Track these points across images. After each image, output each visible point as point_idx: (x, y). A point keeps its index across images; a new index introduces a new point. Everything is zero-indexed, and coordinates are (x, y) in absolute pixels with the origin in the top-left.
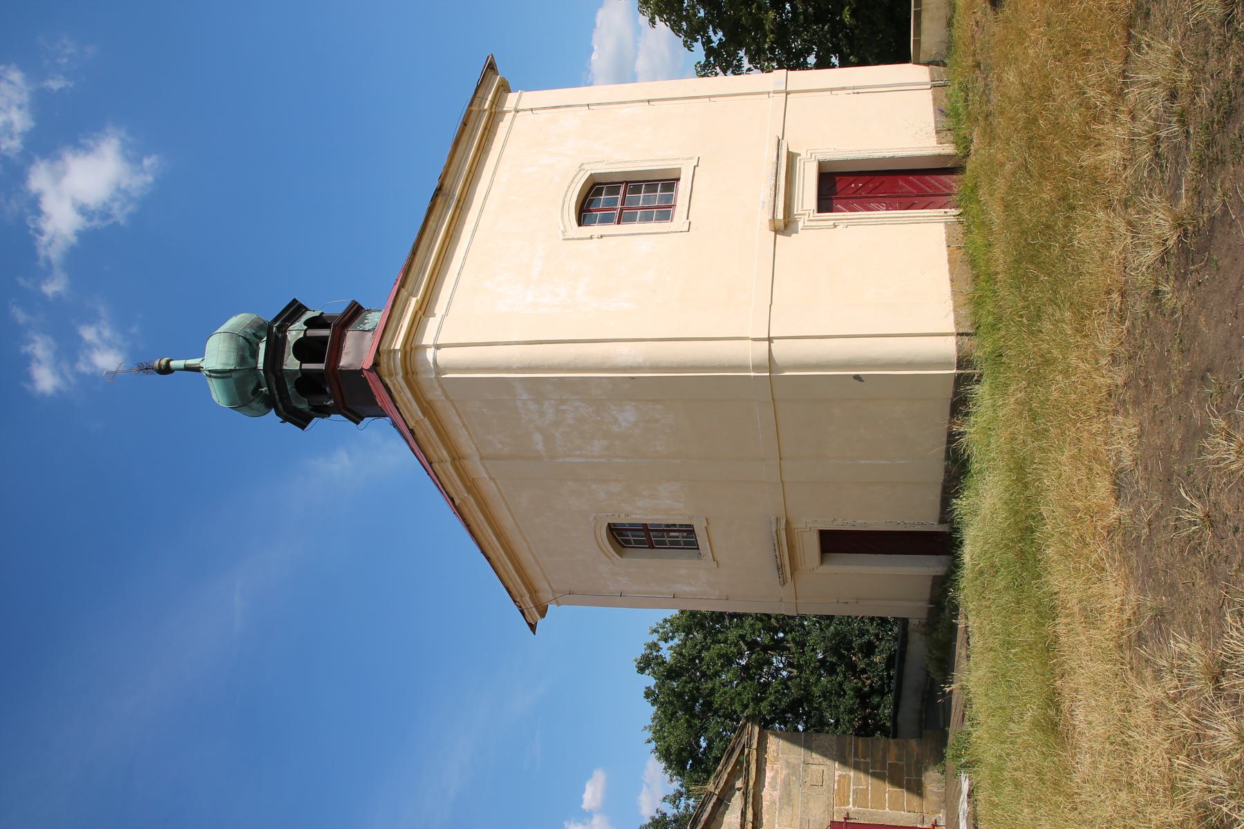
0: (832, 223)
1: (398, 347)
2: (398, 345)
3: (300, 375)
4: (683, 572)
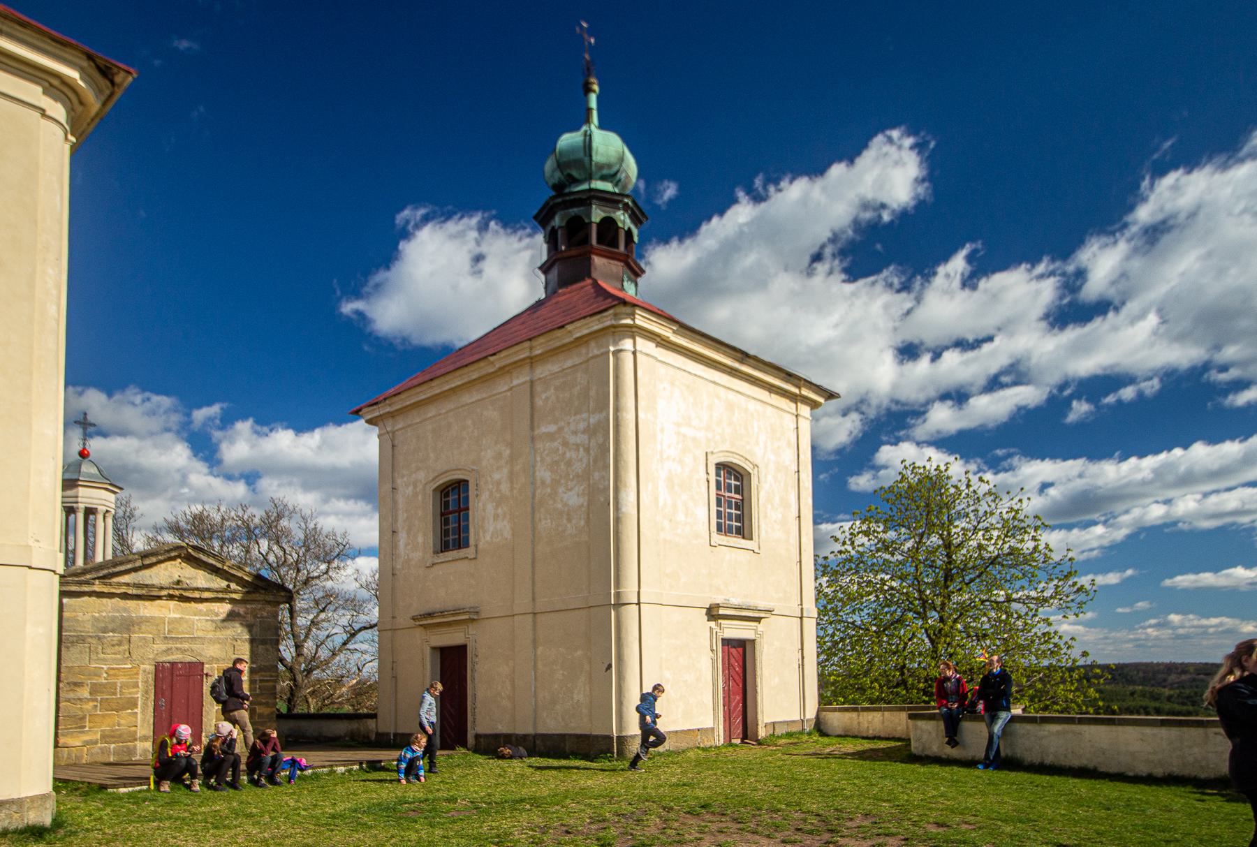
0: (715, 648)
1: (638, 322)
2: (639, 321)
4: (420, 539)
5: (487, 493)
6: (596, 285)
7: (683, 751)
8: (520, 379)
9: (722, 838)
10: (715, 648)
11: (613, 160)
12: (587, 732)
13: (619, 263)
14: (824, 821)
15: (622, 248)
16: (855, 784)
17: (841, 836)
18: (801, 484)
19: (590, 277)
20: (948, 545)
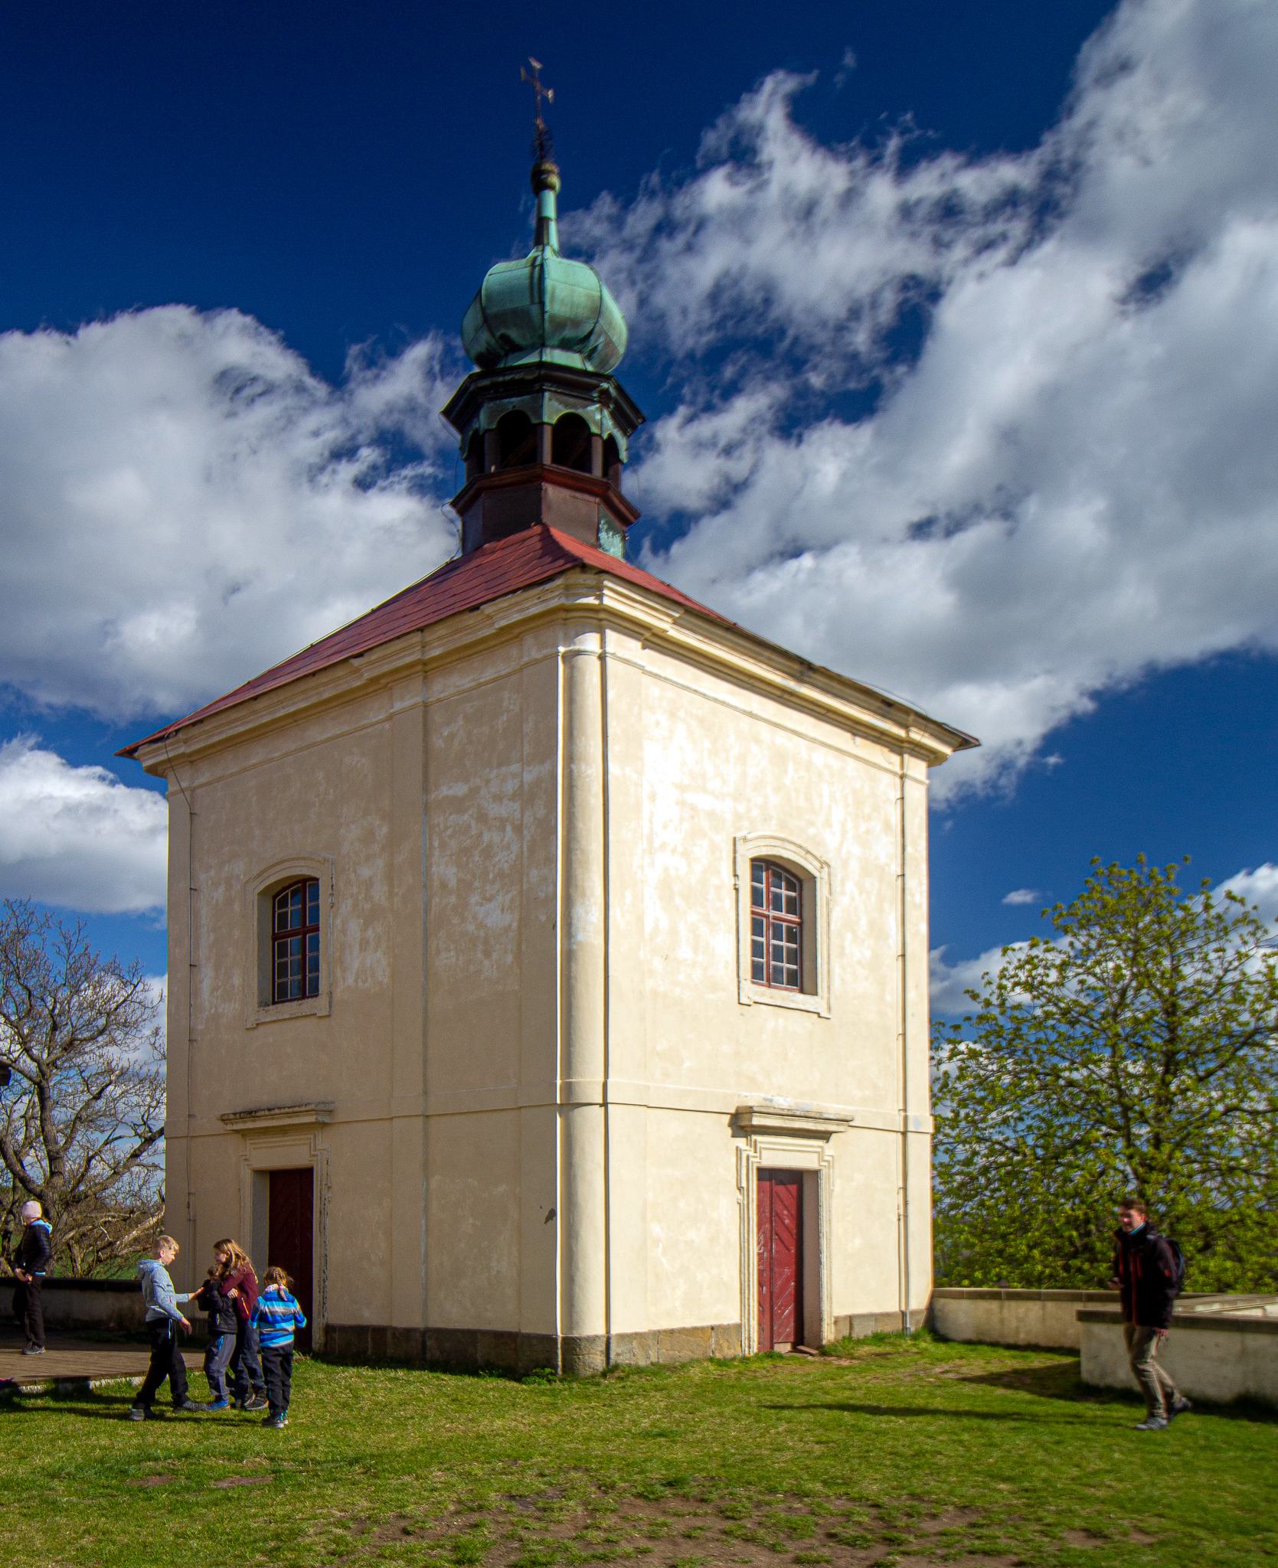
0: (744, 1184)
1: (607, 601)
2: (610, 601)
3: (534, 421)
4: (237, 981)
5: (350, 902)
6: (546, 536)
7: (683, 1366)
8: (406, 700)
9: (687, 1550)
10: (744, 1184)
11: (582, 312)
12: (511, 1327)
13: (592, 499)
14: (882, 1519)
15: (597, 471)
16: (961, 1442)
17: (905, 1553)
18: (908, 898)
19: (539, 522)
20: (1171, 1010)
